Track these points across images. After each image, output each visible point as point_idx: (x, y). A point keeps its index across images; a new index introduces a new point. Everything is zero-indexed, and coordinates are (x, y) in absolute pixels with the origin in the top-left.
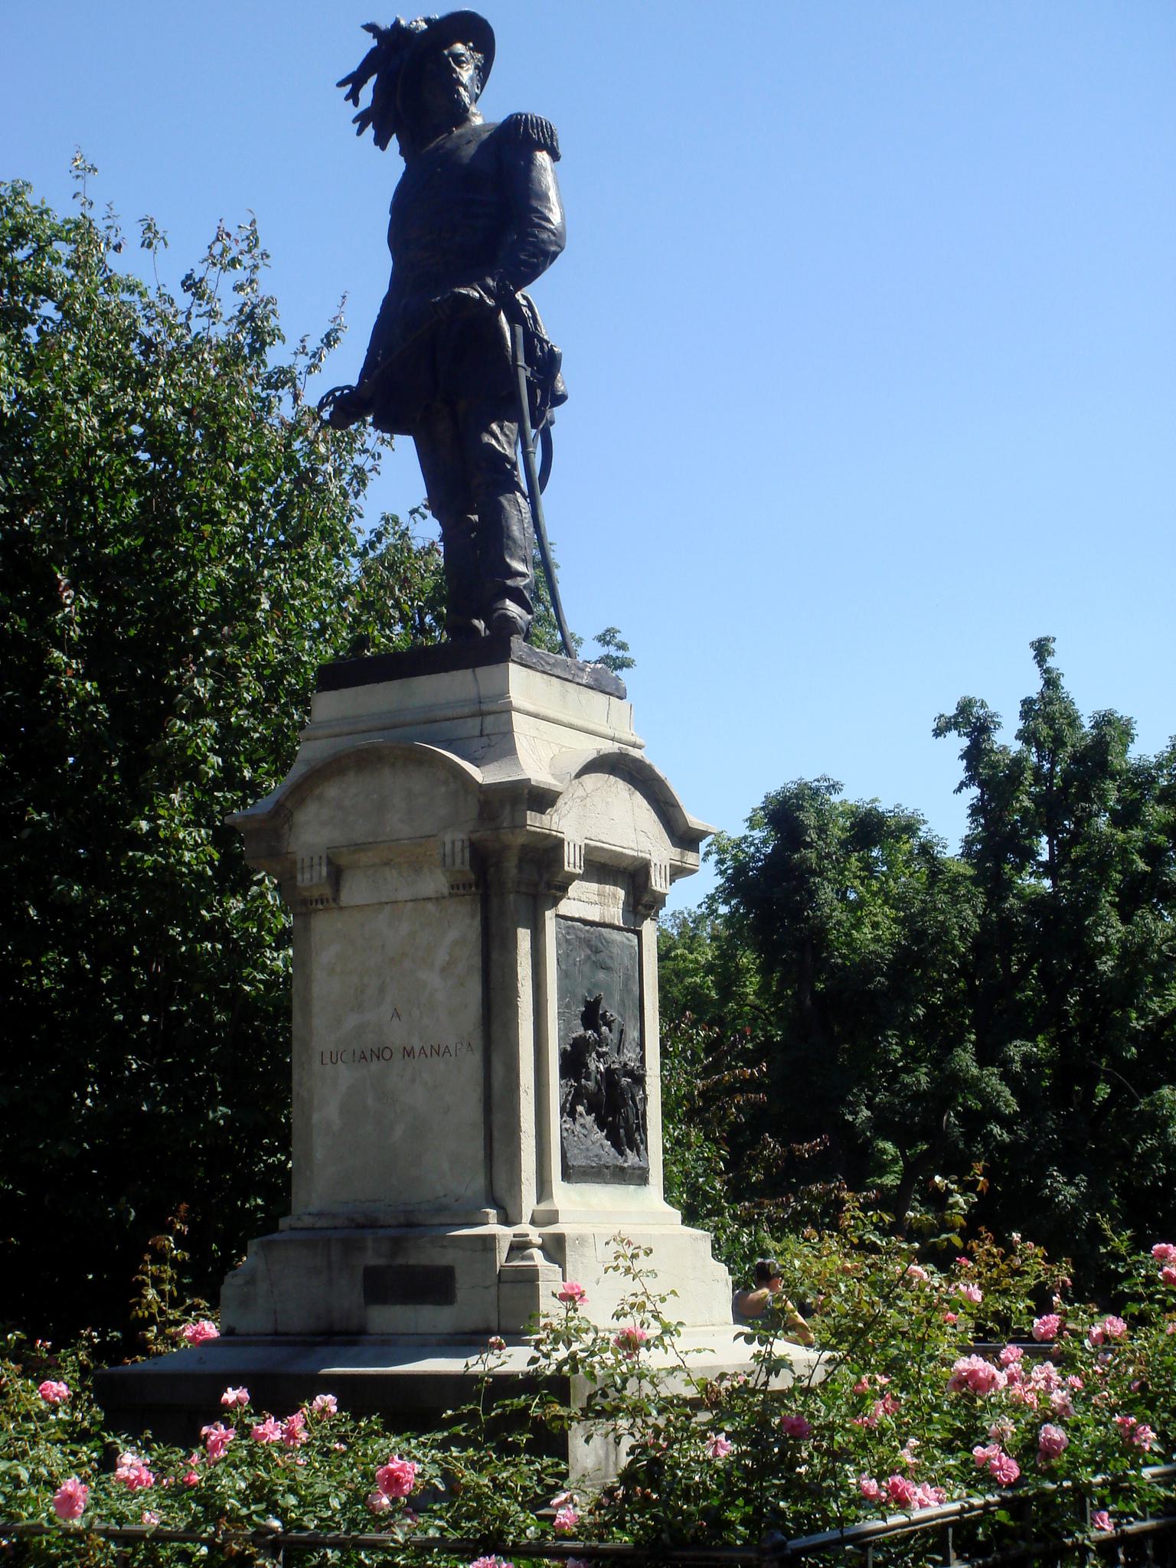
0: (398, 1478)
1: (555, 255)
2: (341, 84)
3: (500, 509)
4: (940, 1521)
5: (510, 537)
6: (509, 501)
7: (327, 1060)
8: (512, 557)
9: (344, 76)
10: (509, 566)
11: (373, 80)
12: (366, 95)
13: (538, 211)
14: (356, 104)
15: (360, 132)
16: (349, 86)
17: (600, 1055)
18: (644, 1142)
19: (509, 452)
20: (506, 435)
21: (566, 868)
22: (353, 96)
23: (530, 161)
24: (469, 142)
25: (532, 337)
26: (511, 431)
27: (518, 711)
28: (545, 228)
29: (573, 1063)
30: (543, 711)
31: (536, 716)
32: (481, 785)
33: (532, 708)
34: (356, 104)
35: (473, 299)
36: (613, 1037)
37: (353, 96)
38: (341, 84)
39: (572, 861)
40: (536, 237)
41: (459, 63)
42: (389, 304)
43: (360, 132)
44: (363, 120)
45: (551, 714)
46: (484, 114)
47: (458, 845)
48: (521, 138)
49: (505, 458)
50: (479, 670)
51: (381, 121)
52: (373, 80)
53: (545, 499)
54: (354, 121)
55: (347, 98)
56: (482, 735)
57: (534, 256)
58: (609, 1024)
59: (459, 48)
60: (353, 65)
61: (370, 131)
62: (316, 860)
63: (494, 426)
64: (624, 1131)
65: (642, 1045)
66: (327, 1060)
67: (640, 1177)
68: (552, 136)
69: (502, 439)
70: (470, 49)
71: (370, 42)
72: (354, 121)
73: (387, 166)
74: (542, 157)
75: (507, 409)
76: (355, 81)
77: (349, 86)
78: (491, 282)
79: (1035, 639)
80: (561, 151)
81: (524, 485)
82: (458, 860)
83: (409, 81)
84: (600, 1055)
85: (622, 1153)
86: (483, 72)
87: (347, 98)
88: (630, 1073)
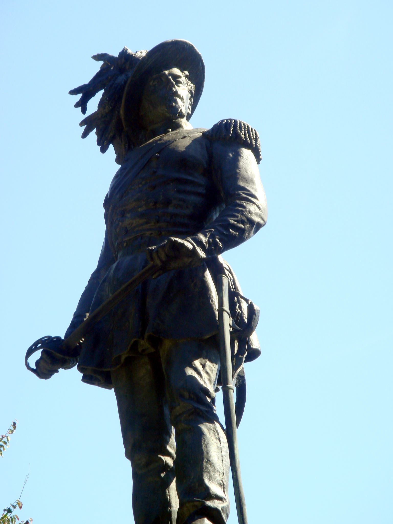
2: (74, 92)
3: (199, 436)
5: (209, 461)
6: (209, 429)
8: (210, 479)
9: (76, 86)
10: (207, 489)
11: (100, 95)
12: (93, 105)
13: (243, 189)
14: (84, 111)
15: (85, 135)
16: (80, 96)
19: (211, 388)
20: (207, 373)
23: (237, 155)
24: (184, 137)
26: (212, 371)
28: (253, 202)
34: (84, 111)
35: (187, 248)
37: (82, 105)
38: (74, 92)
40: (244, 207)
41: (178, 83)
42: (96, 277)
43: (85, 135)
46: (195, 124)
48: (228, 139)
49: (206, 392)
52: (100, 95)
53: (240, 433)
55: (77, 105)
57: (243, 222)
59: (176, 71)
60: (86, 79)
61: (93, 136)
63: (197, 363)
68: (256, 140)
69: (204, 373)
70: (186, 76)
71: (98, 66)
72: (82, 124)
73: (105, 166)
74: (247, 154)
75: (211, 346)
76: (86, 92)
77: (80, 96)
78: (203, 239)
81: (222, 419)
83: (132, 98)
86: (196, 96)
87: (77, 105)
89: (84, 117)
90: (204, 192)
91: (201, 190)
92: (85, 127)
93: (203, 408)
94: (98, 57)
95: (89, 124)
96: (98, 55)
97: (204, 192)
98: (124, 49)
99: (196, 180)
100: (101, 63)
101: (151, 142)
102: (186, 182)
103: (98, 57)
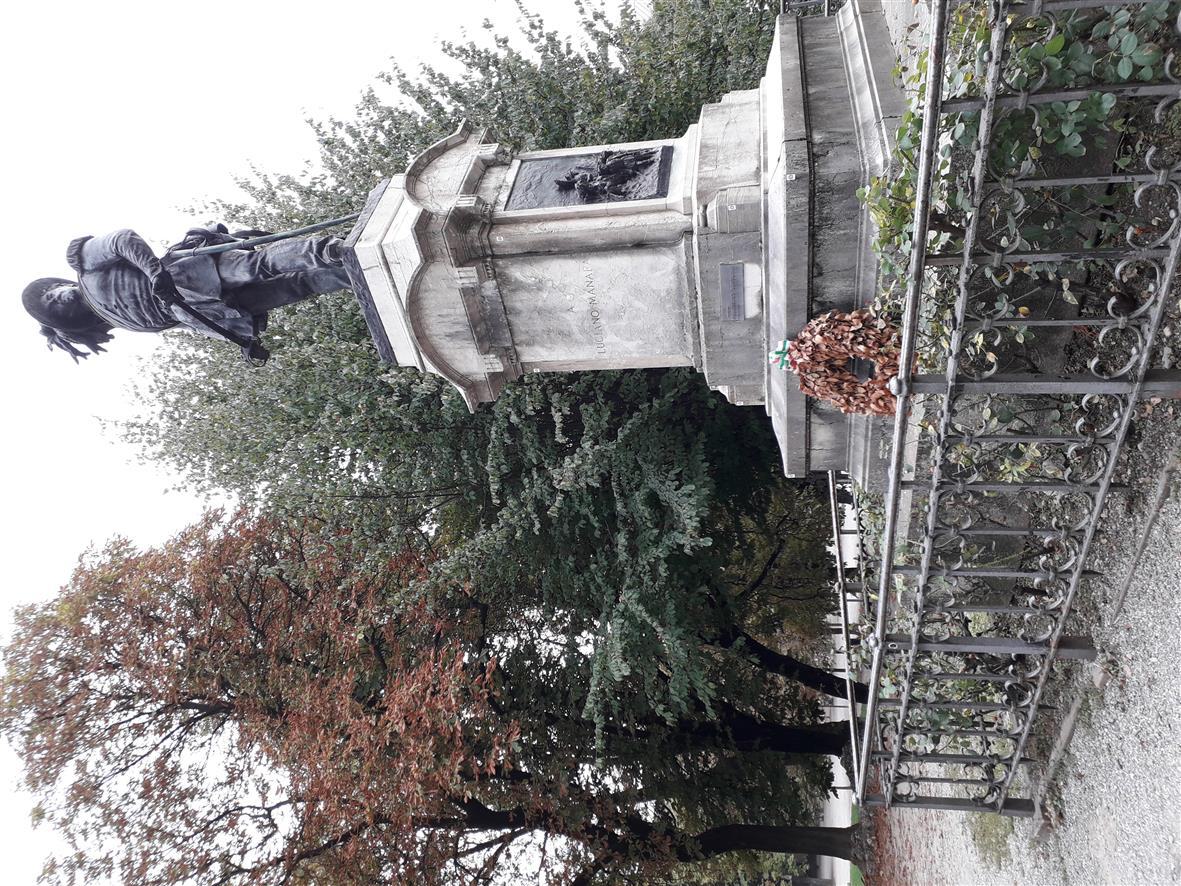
0: (812, 636)
1: (133, 234)
2: (77, 361)
4: (868, 454)
7: (602, 350)
12: (82, 348)
15: (105, 351)
17: (591, 179)
18: (647, 150)
25: (184, 245)
29: (591, 195)
30: (386, 226)
33: (381, 234)
36: (582, 173)
37: (84, 355)
38: (77, 361)
39: (468, 202)
43: (105, 351)
44: (96, 349)
45: (389, 220)
48: (77, 253)
58: (573, 175)
60: (67, 355)
61: (103, 345)
64: (643, 160)
65: (589, 156)
66: (602, 350)
67: (668, 152)
76: (75, 353)
82: (471, 274)
84: (591, 179)
85: (653, 162)
88: (604, 161)
89: (93, 353)
91: (120, 273)
102: (116, 285)
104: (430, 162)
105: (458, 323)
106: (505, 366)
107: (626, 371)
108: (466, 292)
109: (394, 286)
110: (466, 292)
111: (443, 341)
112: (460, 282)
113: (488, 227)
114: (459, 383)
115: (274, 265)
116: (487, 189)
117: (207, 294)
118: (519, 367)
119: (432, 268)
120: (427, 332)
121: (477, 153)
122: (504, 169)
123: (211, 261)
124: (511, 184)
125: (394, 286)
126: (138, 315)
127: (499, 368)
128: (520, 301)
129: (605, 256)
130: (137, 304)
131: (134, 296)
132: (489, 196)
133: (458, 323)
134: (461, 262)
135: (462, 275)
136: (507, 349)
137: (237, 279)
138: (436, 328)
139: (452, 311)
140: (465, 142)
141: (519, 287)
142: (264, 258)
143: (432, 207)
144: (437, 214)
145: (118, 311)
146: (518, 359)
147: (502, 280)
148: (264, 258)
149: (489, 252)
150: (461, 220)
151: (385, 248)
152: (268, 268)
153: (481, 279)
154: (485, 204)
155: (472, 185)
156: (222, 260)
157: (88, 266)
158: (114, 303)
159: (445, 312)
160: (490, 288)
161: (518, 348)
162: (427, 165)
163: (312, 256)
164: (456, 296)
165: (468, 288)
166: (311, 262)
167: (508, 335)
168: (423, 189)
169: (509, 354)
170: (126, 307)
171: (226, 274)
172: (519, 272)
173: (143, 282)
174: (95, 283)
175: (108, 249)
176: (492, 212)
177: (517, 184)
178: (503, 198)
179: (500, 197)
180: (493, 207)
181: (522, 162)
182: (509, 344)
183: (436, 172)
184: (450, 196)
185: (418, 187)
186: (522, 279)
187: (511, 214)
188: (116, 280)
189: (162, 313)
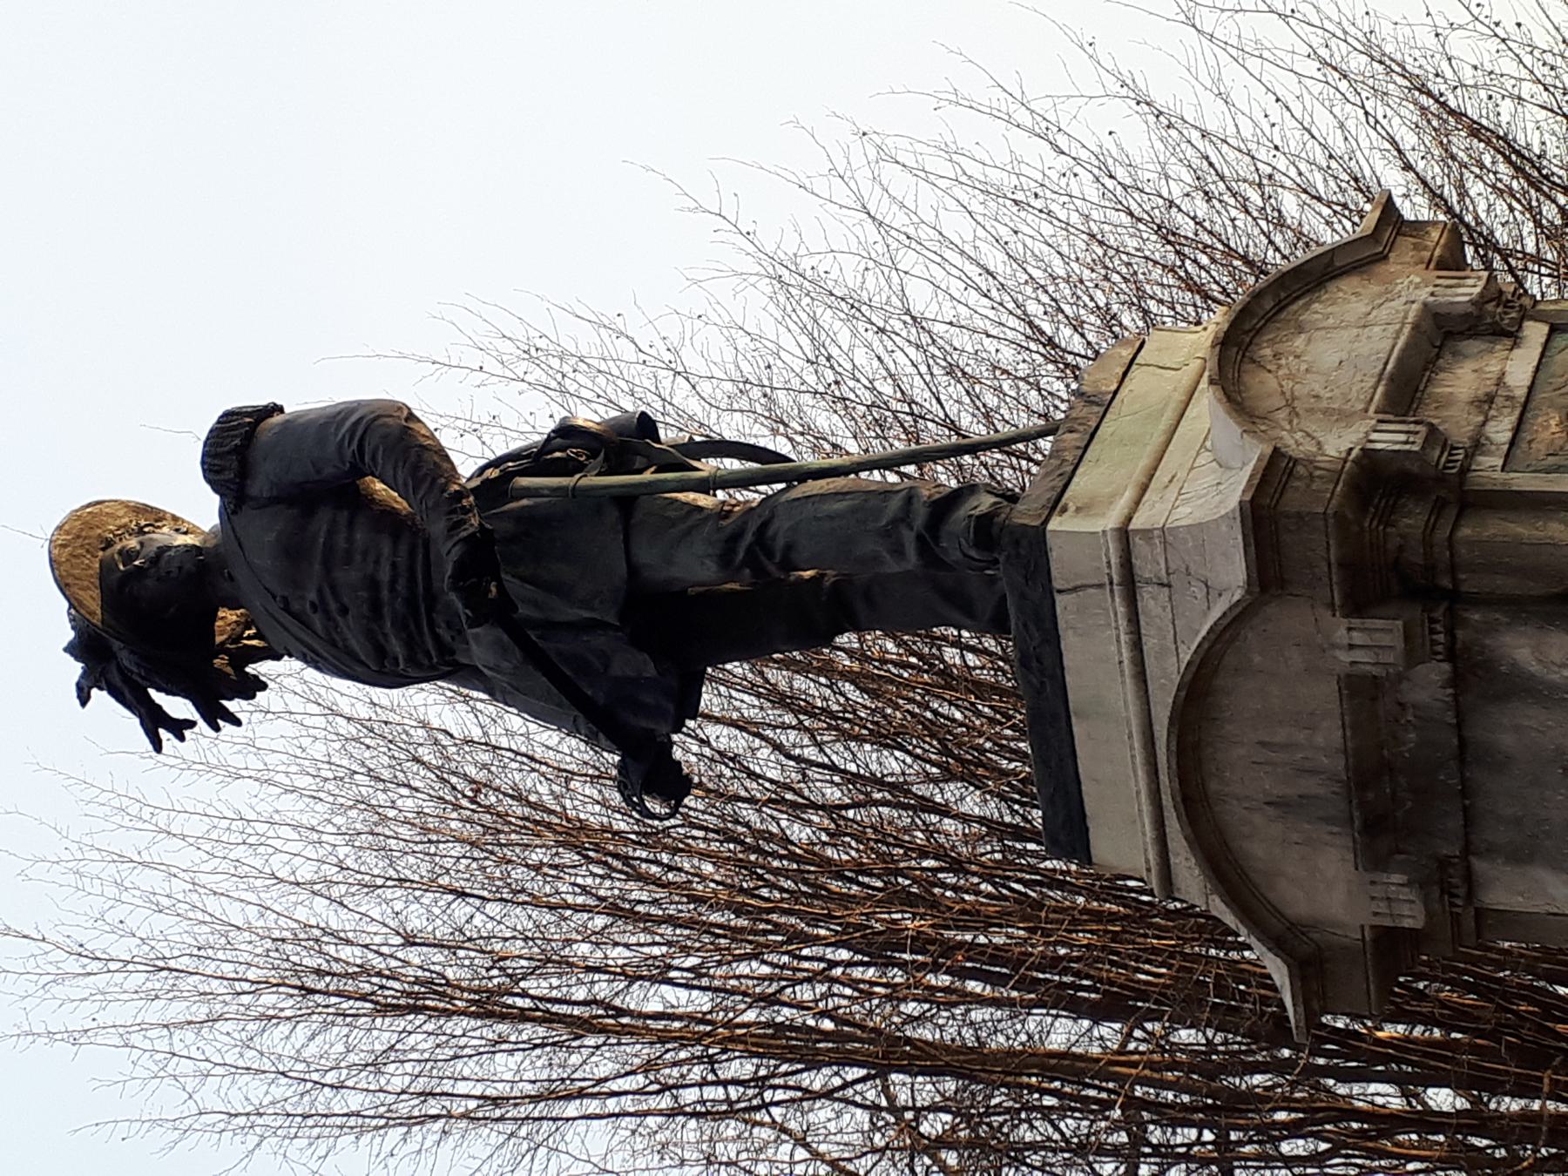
2: (157, 745)
11: (158, 697)
12: (178, 707)
14: (191, 724)
15: (237, 722)
16: (162, 732)
21: (1416, 448)
22: (179, 728)
27: (1129, 519)
30: (1138, 476)
31: (1144, 488)
32: (222, 496)
34: (191, 724)
37: (179, 728)
38: (157, 745)
43: (237, 722)
45: (1144, 462)
47: (1357, 637)
48: (237, 448)
50: (1057, 585)
51: (219, 688)
52: (158, 697)
54: (217, 729)
55: (182, 738)
56: (1169, 586)
62: (1377, 891)
71: (99, 696)
72: (217, 729)
76: (155, 722)
77: (162, 732)
79: (306, 388)
80: (262, 401)
82: (1386, 640)
83: (155, 630)
87: (182, 738)
89: (202, 725)
90: (346, 513)
91: (343, 516)
92: (221, 723)
93: (752, 527)
94: (84, 699)
95: (215, 715)
96: (79, 697)
97: (346, 513)
98: (66, 650)
99: (325, 528)
100: (94, 692)
101: (1066, 1003)
102: (329, 548)
103: (84, 699)
104: (1281, 307)
105: (1312, 772)
106: (1429, 914)
107: (442, 449)
108: (1362, 691)
109: (1137, 645)
110: (1362, 691)
111: (1257, 818)
112: (1345, 657)
113: (1451, 513)
114: (1277, 944)
115: (789, 548)
116: (1446, 402)
117: (585, 604)
118: (1469, 923)
119: (1271, 610)
120: (1213, 786)
121: (1423, 295)
122: (1500, 346)
123: (612, 515)
124: (1521, 393)
125: (1137, 645)
126: (370, 635)
127: (1412, 916)
128: (1513, 730)
129: (1219, 400)
130: (376, 607)
131: (373, 584)
132: (1459, 424)
133: (1312, 772)
134: (1357, 605)
135: (1357, 637)
136: (1444, 863)
137: (676, 572)
138: (1243, 778)
139: (1301, 737)
140: (1383, 258)
141: (1523, 688)
142: (765, 525)
143: (1295, 443)
144: (1310, 462)
145: (317, 621)
146: (1470, 896)
147: (1475, 677)
148: (765, 525)
149: (1446, 582)
150: (1373, 477)
151: (1137, 541)
152: (770, 555)
153: (1412, 657)
154: (1447, 446)
155: (1406, 388)
156: (638, 516)
157: (259, 487)
158: (312, 596)
159: (1281, 735)
160: (1429, 684)
161: (1479, 865)
162: (1271, 318)
163: (909, 538)
164: (1324, 694)
165: (1363, 677)
166: (898, 552)
167: (1455, 824)
168: (1264, 385)
169: (1450, 882)
170: (344, 611)
171: (646, 554)
172: (1526, 649)
173: (403, 548)
174: (271, 537)
175: (332, 448)
176: (1465, 470)
177: (1539, 396)
178: (1500, 430)
179: (1490, 429)
180: (1470, 456)
181: (1554, 330)
182: (1451, 849)
183: (1299, 342)
184: (1344, 417)
185: (1246, 378)
186: (1535, 668)
187: (1524, 481)
188: (330, 533)
189: (437, 638)
